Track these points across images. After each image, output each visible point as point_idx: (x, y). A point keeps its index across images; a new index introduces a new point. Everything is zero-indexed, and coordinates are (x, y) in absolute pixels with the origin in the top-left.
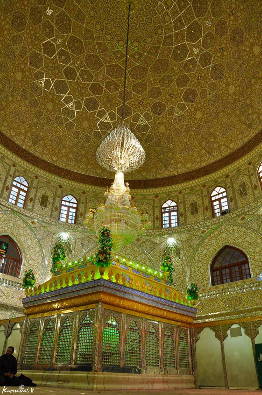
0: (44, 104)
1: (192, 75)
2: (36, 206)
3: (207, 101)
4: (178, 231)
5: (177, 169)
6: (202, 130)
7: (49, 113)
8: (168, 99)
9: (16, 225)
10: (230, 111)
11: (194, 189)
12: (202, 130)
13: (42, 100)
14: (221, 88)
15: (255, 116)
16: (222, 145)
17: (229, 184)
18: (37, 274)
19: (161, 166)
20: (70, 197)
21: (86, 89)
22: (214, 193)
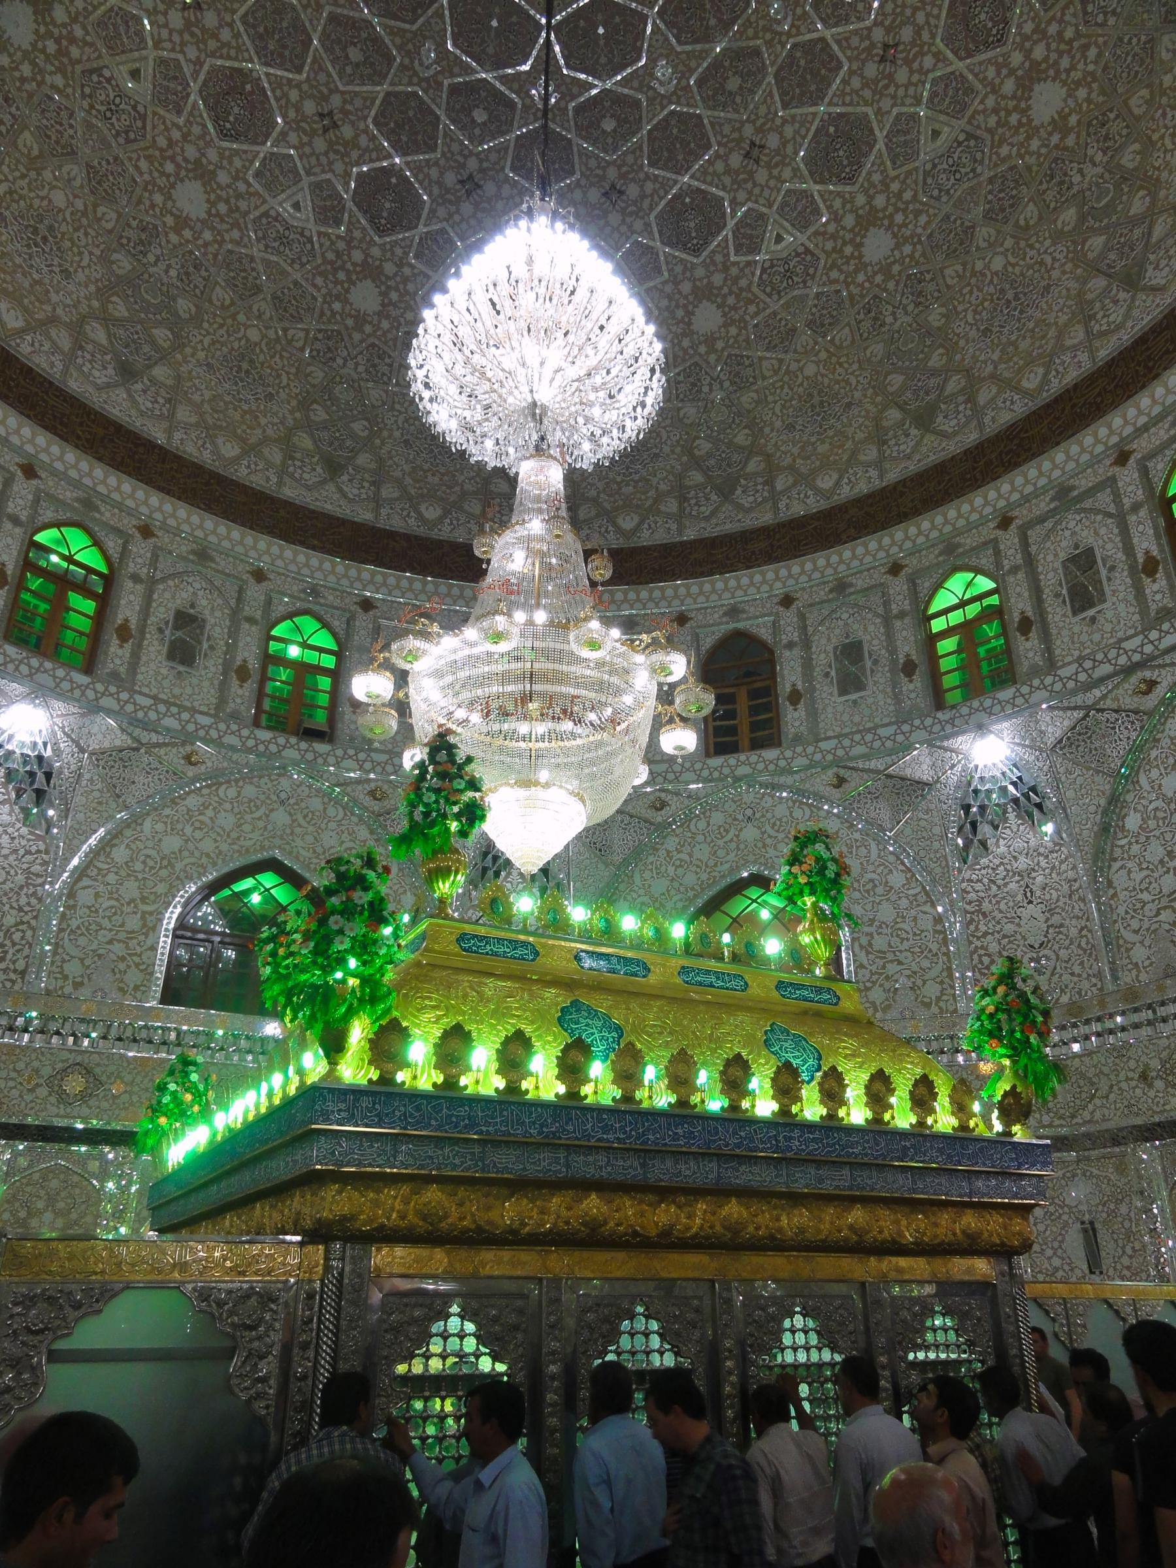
0: (160, 189)
1: (855, 41)
3: (921, 172)
4: (83, 694)
5: (774, 497)
6: (889, 320)
7: (187, 234)
8: (737, 172)
10: (1030, 212)
11: (851, 585)
12: (889, 320)
13: (152, 164)
14: (990, 102)
15: (954, 384)
16: (984, 379)
17: (1012, 555)
19: (700, 487)
20: (308, 624)
21: (359, 119)
22: (942, 600)
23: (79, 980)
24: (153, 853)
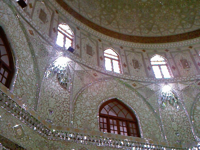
2: (131, 70)
9: (121, 89)
18: (156, 134)
23: (81, 125)
24: (91, 96)
